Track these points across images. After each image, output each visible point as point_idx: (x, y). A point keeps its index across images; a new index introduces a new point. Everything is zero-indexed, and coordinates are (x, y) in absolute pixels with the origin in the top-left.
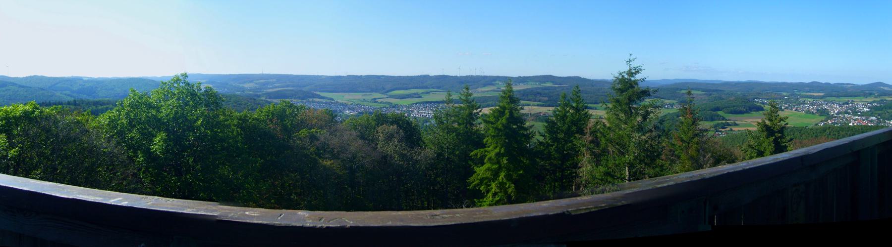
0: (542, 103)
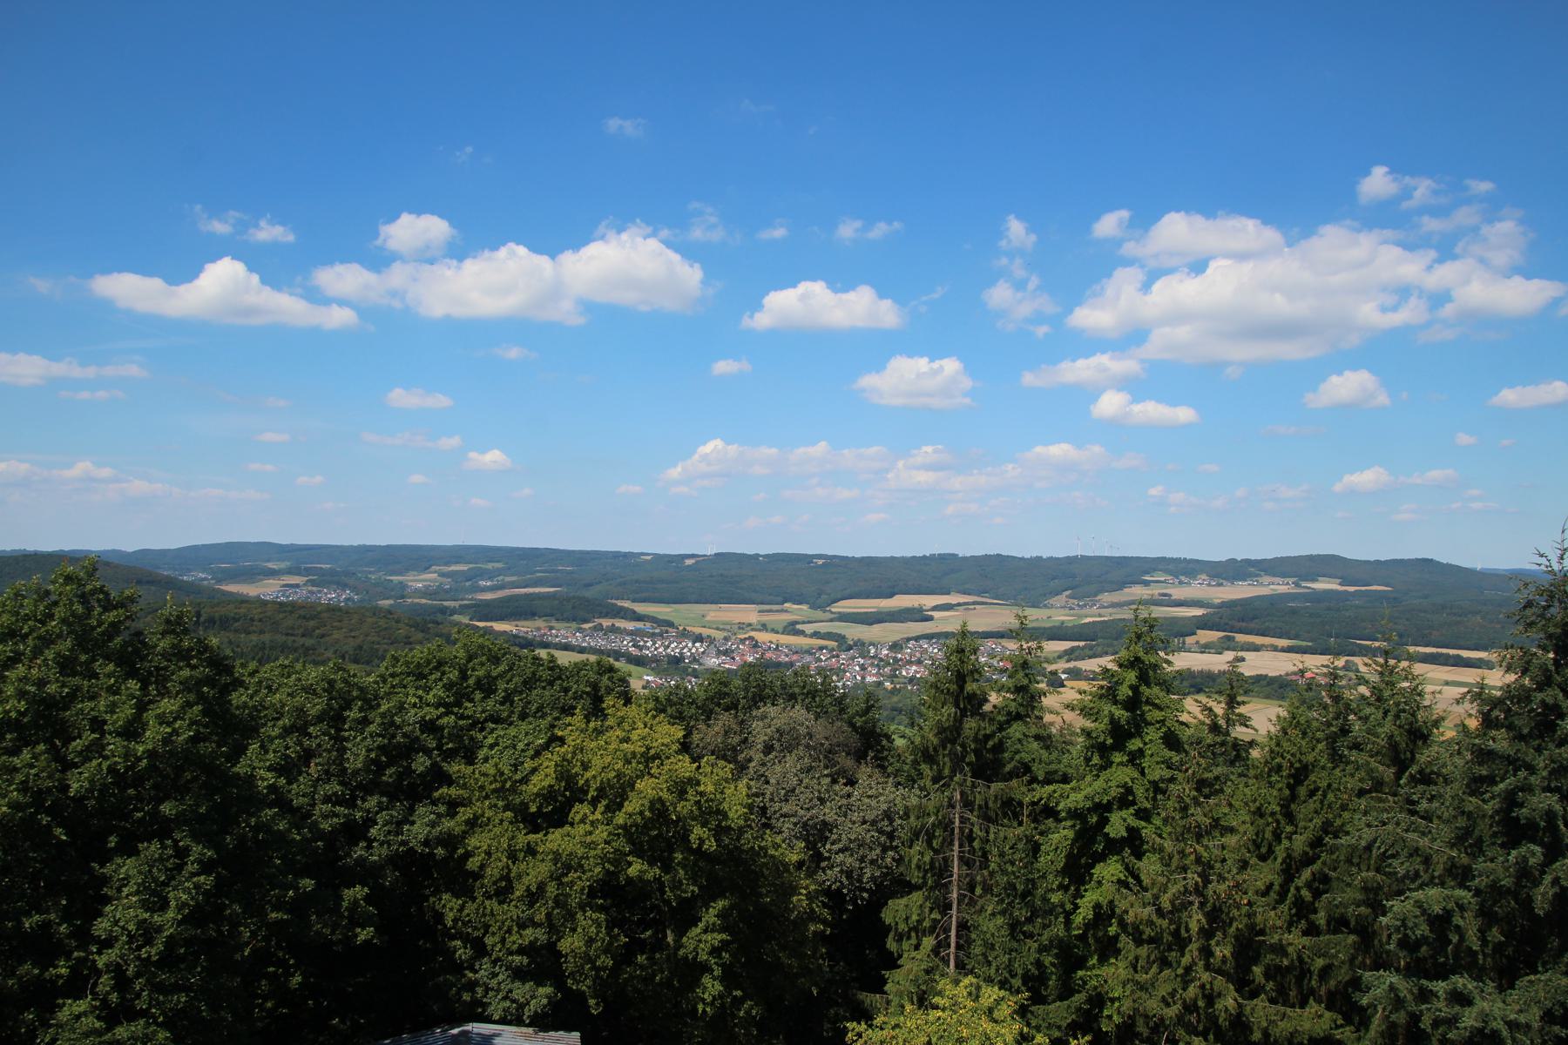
0: (1304, 643)
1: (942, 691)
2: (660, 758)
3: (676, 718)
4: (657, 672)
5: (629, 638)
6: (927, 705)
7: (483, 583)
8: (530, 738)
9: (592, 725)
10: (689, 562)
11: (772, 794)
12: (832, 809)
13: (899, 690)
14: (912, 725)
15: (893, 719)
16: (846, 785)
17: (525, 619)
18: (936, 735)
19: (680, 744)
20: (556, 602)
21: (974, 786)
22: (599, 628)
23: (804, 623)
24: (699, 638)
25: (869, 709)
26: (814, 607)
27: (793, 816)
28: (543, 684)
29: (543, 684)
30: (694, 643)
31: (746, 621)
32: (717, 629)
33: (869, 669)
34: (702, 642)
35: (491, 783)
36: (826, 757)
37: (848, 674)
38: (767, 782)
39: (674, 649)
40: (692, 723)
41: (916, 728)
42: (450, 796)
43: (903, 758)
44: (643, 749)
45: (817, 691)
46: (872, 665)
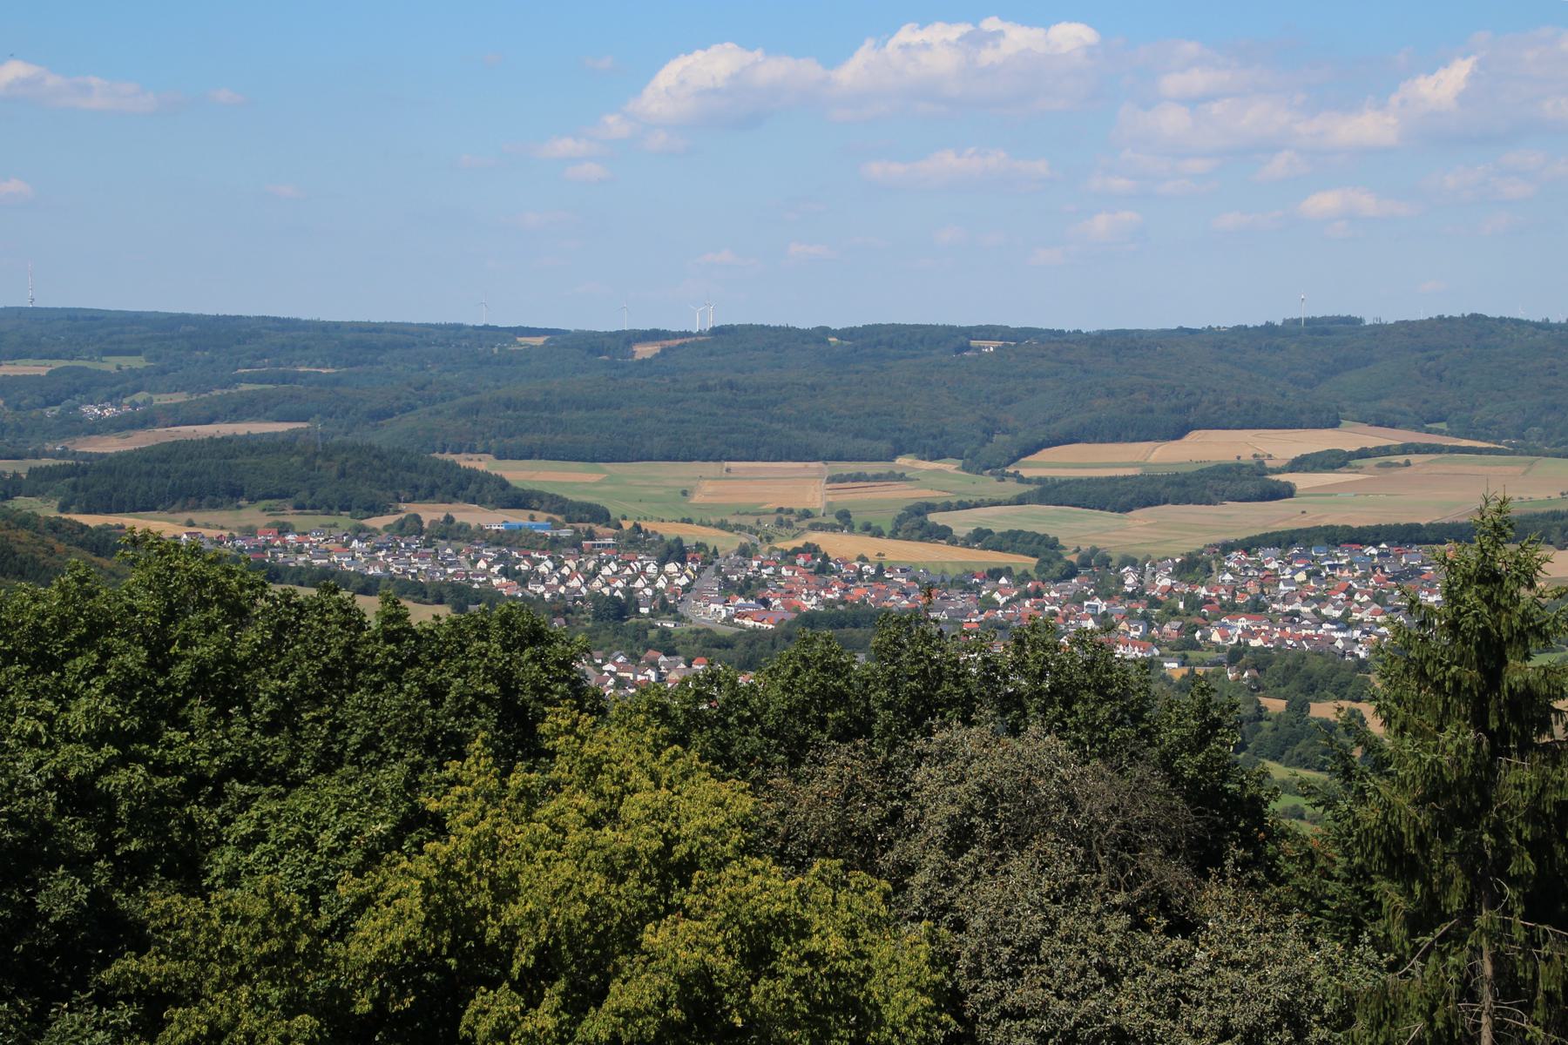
5: (490, 553)
7: (91, 411)
8: (351, 819)
9: (515, 781)
10: (645, 351)
11: (976, 956)
12: (1137, 997)
16: (1170, 931)
17: (214, 506)
18: (1419, 802)
20: (296, 460)
21: (1532, 941)
22: (411, 527)
23: (948, 507)
24: (676, 552)
26: (976, 464)
27: (1035, 1013)
30: (662, 563)
31: (799, 506)
32: (723, 526)
33: (1123, 626)
34: (683, 561)
35: (256, 942)
36: (1114, 859)
38: (959, 926)
39: (610, 581)
42: (146, 979)
43: (1322, 863)
44: (657, 844)
46: (1130, 615)
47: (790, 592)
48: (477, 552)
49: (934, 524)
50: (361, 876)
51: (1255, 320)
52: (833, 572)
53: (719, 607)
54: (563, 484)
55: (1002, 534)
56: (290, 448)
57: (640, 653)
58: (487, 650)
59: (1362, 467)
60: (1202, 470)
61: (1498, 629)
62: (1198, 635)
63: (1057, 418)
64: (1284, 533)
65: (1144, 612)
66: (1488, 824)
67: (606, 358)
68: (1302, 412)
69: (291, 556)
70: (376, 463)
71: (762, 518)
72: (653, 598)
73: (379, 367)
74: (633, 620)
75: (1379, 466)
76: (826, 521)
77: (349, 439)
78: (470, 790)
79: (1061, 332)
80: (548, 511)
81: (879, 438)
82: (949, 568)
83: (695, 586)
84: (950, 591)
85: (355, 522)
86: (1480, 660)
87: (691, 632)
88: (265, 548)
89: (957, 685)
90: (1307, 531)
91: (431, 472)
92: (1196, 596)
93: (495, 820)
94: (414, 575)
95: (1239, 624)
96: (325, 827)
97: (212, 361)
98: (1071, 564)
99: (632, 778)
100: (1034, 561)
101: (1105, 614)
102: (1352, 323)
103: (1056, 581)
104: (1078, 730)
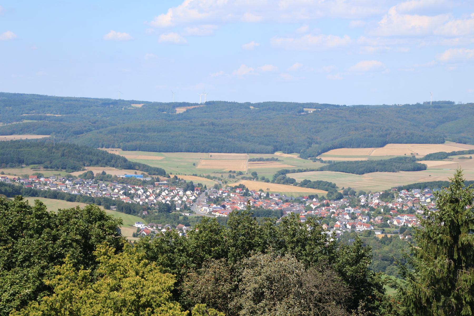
1: (435, 241)
2: (150, 306)
3: (168, 266)
4: (149, 220)
5: (119, 186)
6: (419, 255)
8: (16, 288)
9: (81, 273)
10: (180, 110)
13: (391, 240)
14: (404, 275)
15: (384, 268)
17: (12, 167)
19: (171, 292)
20: (45, 150)
22: (90, 176)
23: (294, 171)
24: (190, 187)
25: (360, 257)
26: (304, 156)
28: (31, 232)
29: (31, 232)
30: (185, 191)
31: (238, 170)
32: (208, 177)
33: (360, 218)
34: (193, 190)
36: (316, 305)
37: (338, 223)
40: (183, 271)
41: (408, 278)
43: (394, 309)
44: (134, 298)
45: (306, 239)
46: (362, 214)
47: (234, 203)
48: (114, 186)
49: (289, 178)
50: (19, 311)
51: (412, 102)
52: (250, 195)
53: (206, 208)
54: (148, 160)
55: (314, 182)
56: (43, 145)
57: (176, 225)
58: (77, 222)
59: (453, 159)
60: (391, 159)
61: (457, 220)
62: (388, 222)
63: (336, 138)
64: (422, 183)
65: (368, 213)
66: (454, 295)
67: (165, 113)
68: (430, 137)
69: (42, 186)
70: (76, 151)
71: (224, 175)
72: (181, 204)
73: (78, 114)
74: (174, 212)
75: (460, 158)
76: (248, 176)
77: (66, 142)
78: (63, 276)
79: (338, 106)
80: (142, 171)
81: (269, 145)
82: (294, 195)
83: (197, 200)
84: (294, 203)
85: (68, 173)
86: (450, 232)
87: (195, 217)
88: (32, 183)
89: (260, 238)
90: (431, 183)
91: (97, 155)
92: (388, 207)
93: (71, 288)
94: (90, 194)
95: (404, 218)
96: (5, 291)
97: (13, 111)
98: (340, 194)
99: (128, 273)
100: (327, 192)
101: (353, 213)
102: (450, 104)
103: (335, 200)
104: (306, 256)
